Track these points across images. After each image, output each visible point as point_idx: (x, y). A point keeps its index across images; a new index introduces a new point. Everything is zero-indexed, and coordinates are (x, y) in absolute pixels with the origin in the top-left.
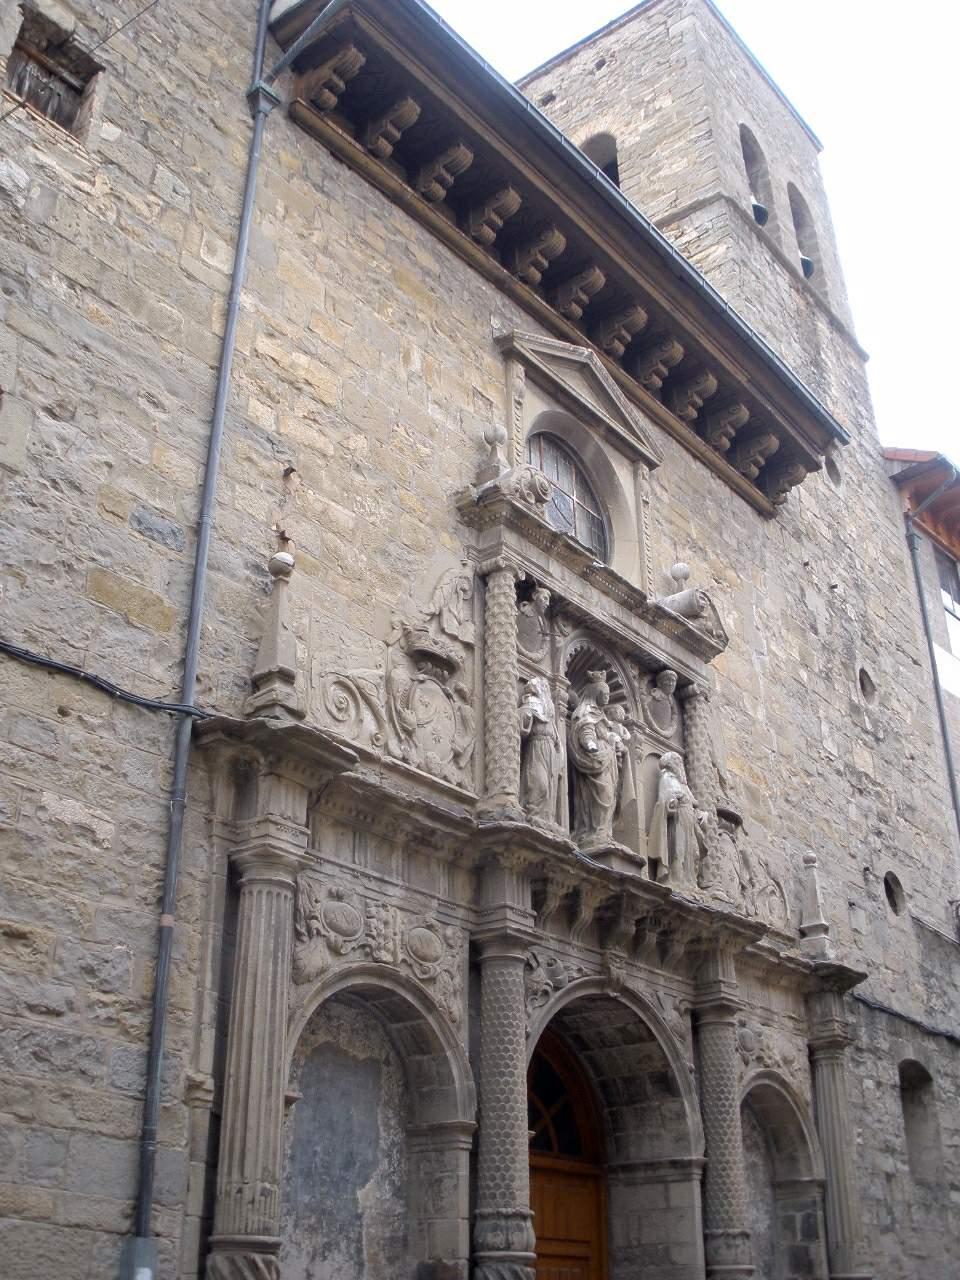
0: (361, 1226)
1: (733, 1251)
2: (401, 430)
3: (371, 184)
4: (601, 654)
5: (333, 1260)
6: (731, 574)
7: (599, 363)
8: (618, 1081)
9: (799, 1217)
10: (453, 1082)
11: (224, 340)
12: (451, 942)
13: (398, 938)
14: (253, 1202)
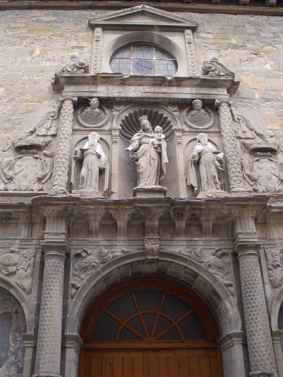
3: (19, 9)
7: (149, 7)
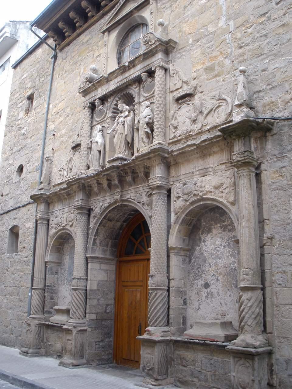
4: (125, 93)
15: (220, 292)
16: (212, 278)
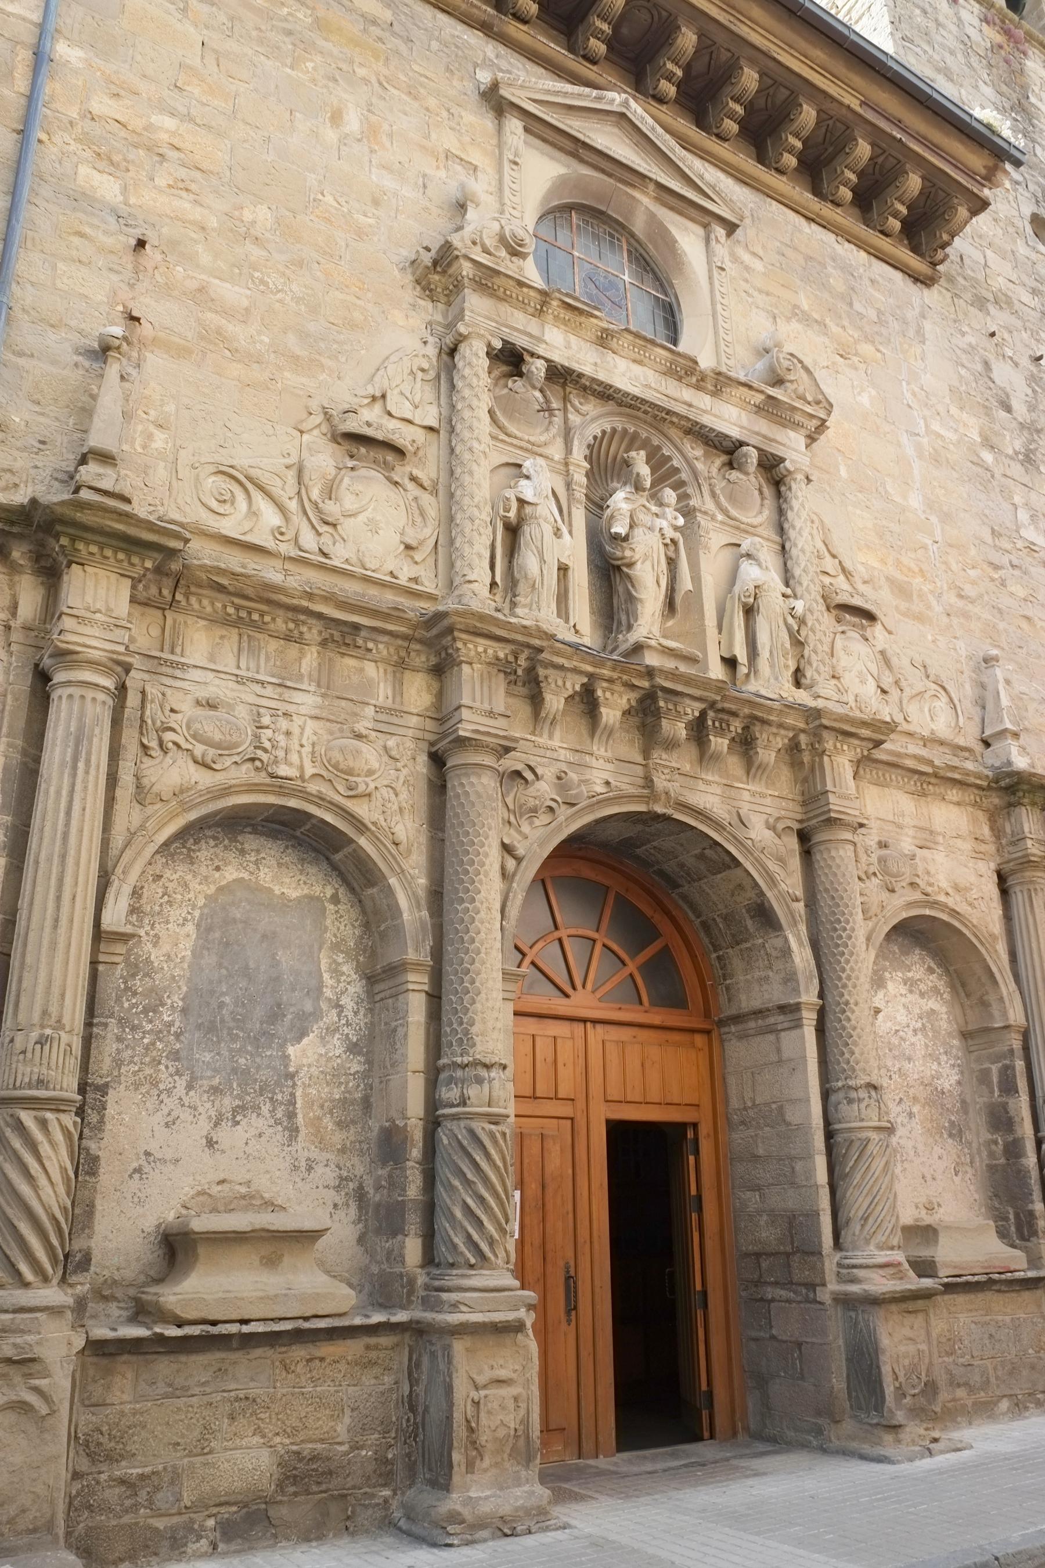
0: (294, 1085)
1: (855, 1106)
2: (329, 199)
5: (249, 1124)
6: (867, 349)
7: (639, 110)
8: (718, 920)
9: (995, 1069)
10: (401, 914)
11: (31, 98)
12: (393, 753)
13: (308, 749)
14: (24, 1052)
15: (921, 1147)
16: (899, 1109)
